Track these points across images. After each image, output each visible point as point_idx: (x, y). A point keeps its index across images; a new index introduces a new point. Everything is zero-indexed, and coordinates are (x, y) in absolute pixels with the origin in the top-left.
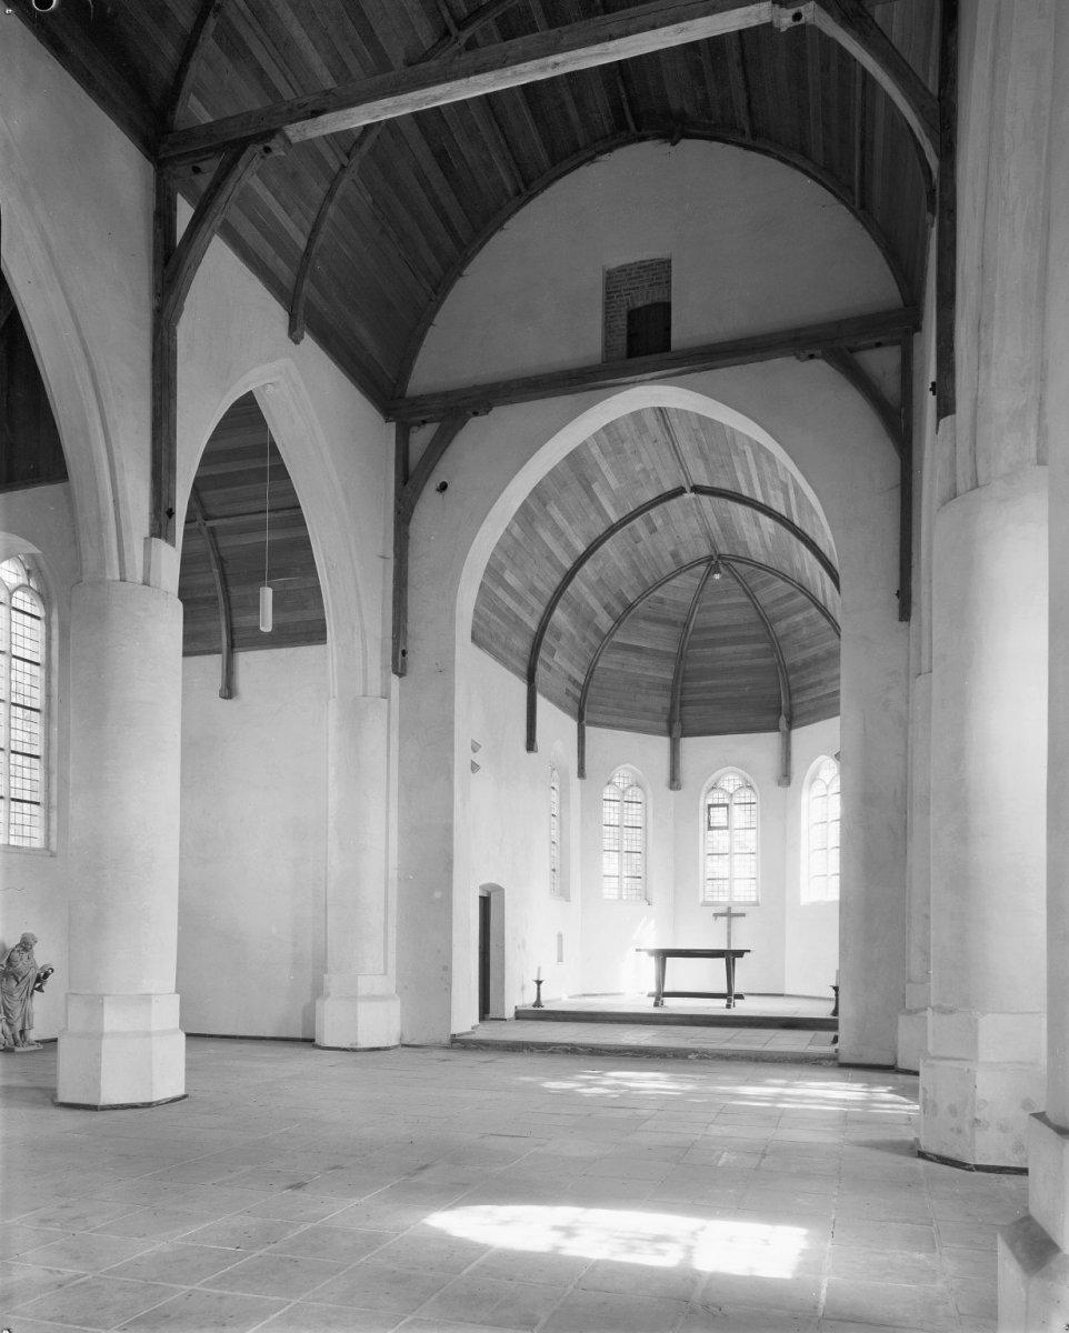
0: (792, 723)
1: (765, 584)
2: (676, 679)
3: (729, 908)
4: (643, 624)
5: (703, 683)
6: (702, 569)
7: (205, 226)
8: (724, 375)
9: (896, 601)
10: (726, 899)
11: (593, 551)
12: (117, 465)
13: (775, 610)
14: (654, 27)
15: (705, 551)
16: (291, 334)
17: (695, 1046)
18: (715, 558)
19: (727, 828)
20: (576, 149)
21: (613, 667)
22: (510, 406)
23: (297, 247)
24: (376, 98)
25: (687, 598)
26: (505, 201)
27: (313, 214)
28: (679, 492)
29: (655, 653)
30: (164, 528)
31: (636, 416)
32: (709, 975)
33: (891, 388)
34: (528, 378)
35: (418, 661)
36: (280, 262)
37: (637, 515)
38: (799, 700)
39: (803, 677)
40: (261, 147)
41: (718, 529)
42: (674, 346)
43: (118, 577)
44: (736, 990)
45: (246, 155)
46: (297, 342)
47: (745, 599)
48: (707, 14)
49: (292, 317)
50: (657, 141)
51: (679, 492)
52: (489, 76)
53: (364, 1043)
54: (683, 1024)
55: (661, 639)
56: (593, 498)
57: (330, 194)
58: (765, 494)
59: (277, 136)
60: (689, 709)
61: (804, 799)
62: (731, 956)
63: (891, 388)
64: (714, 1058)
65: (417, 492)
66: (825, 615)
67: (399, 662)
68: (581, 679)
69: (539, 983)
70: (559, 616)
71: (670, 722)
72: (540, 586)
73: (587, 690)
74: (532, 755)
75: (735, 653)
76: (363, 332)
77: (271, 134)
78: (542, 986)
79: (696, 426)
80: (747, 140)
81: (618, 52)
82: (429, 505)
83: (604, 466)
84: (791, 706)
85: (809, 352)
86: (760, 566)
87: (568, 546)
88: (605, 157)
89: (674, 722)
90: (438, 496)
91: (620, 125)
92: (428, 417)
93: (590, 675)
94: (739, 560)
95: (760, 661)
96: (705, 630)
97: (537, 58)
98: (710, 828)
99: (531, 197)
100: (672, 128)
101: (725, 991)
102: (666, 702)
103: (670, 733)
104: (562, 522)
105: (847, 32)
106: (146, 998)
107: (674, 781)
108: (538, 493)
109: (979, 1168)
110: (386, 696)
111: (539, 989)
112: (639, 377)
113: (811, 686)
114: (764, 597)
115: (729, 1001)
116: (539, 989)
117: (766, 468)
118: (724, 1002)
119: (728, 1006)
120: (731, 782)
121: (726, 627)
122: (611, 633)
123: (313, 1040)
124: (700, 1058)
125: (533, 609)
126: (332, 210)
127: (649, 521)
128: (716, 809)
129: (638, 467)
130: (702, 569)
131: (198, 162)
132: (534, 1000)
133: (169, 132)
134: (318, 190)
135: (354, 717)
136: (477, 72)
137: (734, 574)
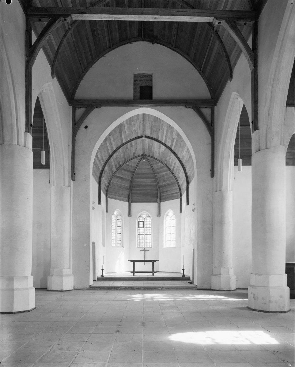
1: (156, 164)
2: (130, 187)
3: (144, 249)
4: (123, 171)
5: (137, 188)
6: (139, 158)
7: (44, 38)
8: (167, 108)
9: (210, 172)
10: (143, 246)
11: (117, 150)
13: (158, 171)
14: (184, 15)
15: (142, 153)
16: (52, 75)
17: (160, 286)
18: (144, 155)
19: (143, 227)
24: (102, 13)
25: (134, 165)
26: (106, 48)
27: (60, 40)
28: (142, 137)
31: (138, 116)
32: (148, 267)
33: (209, 119)
34: (113, 100)
35: (78, 177)
38: (163, 195)
39: (164, 189)
40: (63, 19)
41: (147, 148)
42: (154, 96)
43: (17, 144)
44: (155, 271)
45: (59, 20)
46: (53, 78)
47: (150, 167)
49: (52, 70)
50: (149, 42)
51: (142, 137)
52: (137, 16)
53: (65, 289)
54: (145, 280)
55: (127, 175)
57: (65, 36)
58: (166, 140)
59: (70, 16)
61: (164, 221)
62: (153, 261)
63: (209, 119)
64: (165, 289)
65: (79, 127)
66: (172, 173)
67: (73, 177)
69: (103, 270)
70: (106, 167)
71: (129, 198)
72: (104, 158)
73: (108, 188)
78: (103, 271)
79: (152, 120)
80: (173, 48)
82: (82, 131)
83: (126, 127)
86: (156, 159)
87: (112, 148)
88: (134, 43)
89: (130, 198)
90: (85, 130)
91: (140, 35)
92: (82, 106)
94: (150, 156)
95: (152, 184)
97: (152, 15)
98: (139, 227)
100: (153, 40)
101: (152, 271)
102: (128, 193)
103: (128, 201)
104: (112, 141)
105: (232, 30)
106: (26, 277)
107: (130, 214)
109: (271, 312)
110: (69, 186)
111: (102, 271)
113: (167, 191)
114: (155, 167)
115: (153, 274)
116: (102, 271)
117: (169, 134)
118: (152, 274)
119: (153, 275)
120: (144, 215)
121: (144, 174)
123: (47, 289)
124: (162, 289)
125: (101, 165)
126: (65, 41)
127: (132, 144)
128: (140, 222)
129: (133, 129)
130: (139, 158)
131: (41, 18)
132: (101, 274)
133: (31, 6)
135: (60, 193)
136: (134, 14)
137: (148, 160)
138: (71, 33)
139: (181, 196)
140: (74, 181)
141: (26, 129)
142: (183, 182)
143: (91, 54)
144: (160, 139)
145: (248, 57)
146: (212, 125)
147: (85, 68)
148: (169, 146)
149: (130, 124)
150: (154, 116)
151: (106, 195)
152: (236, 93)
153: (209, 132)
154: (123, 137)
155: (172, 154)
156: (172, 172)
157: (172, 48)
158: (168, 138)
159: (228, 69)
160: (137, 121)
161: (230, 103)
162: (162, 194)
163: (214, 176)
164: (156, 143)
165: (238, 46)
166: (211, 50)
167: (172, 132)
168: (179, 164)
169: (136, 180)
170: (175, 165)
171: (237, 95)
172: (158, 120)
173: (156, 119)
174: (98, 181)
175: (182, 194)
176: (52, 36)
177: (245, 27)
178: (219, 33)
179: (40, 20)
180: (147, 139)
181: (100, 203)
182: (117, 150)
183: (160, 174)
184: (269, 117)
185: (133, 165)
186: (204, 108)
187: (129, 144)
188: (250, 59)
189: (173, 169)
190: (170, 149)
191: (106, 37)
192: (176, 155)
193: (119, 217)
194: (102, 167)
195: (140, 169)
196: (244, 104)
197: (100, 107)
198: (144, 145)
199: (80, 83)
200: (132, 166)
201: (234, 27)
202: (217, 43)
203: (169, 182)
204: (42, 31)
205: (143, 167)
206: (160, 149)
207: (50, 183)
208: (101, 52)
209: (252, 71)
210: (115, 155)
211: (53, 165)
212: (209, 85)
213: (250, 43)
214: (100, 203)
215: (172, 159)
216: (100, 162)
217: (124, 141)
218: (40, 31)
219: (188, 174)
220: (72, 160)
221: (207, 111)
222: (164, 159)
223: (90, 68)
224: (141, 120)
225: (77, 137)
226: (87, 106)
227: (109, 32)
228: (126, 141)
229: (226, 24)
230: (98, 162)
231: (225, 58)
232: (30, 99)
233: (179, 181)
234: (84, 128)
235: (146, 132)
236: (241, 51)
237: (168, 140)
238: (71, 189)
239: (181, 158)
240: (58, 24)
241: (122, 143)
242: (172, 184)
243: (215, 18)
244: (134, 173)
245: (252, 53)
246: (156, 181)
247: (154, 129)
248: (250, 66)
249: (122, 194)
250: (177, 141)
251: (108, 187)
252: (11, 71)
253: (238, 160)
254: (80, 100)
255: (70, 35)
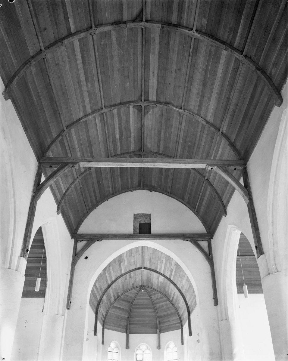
0: (161, 331)
1: (155, 294)
2: (128, 317)
4: (121, 302)
6: (138, 288)
7: (52, 179)
9: (213, 300)
12: (16, 234)
14: (180, 163)
15: (140, 284)
18: (143, 286)
20: (128, 188)
21: (112, 312)
22: (108, 240)
23: (63, 192)
27: (68, 186)
28: (141, 268)
29: (123, 310)
30: (25, 254)
31: (137, 248)
36: (58, 194)
37: (128, 273)
38: (163, 325)
42: (152, 232)
43: (8, 267)
45: (68, 166)
46: (58, 214)
47: (148, 298)
48: (192, 163)
49: (58, 207)
50: (147, 191)
51: (141, 268)
52: (138, 164)
56: (120, 266)
57: (73, 183)
58: (164, 271)
59: (77, 164)
60: (132, 326)
63: (207, 250)
65: (79, 258)
68: (104, 315)
70: (105, 297)
72: (102, 288)
74: (95, 336)
75: (145, 311)
76: (71, 216)
77: (76, 163)
79: (151, 252)
80: (169, 194)
81: (170, 166)
82: (81, 261)
83: (125, 259)
84: (160, 327)
85: (187, 239)
86: (154, 289)
87: (111, 278)
88: (135, 191)
92: (84, 239)
93: (107, 314)
94: (148, 287)
96: (137, 305)
99: (116, 195)
103: (126, 332)
104: (112, 272)
107: (127, 347)
108: (109, 265)
110: (63, 315)
112: (144, 238)
113: (166, 322)
114: (154, 297)
121: (143, 304)
122: (113, 303)
126: (73, 186)
127: (130, 275)
129: (133, 260)
133: (44, 157)
134: (71, 181)
137: (146, 290)
138: (79, 181)
139: (182, 326)
140: (69, 310)
141: (21, 253)
142: (184, 311)
143: (96, 199)
144: (158, 270)
145: (242, 192)
146: (210, 255)
147: (89, 210)
148: (168, 276)
149: (130, 256)
150: (153, 249)
151: (103, 326)
152: (232, 226)
153: (208, 262)
154: (123, 268)
155: (171, 284)
156: (171, 302)
157: (168, 194)
158: (166, 269)
159: (222, 207)
160: (136, 253)
161: (227, 234)
162: (161, 324)
163: (218, 304)
164: (155, 273)
165: (231, 185)
166: (204, 194)
167: (170, 263)
168: (179, 293)
169: (135, 310)
170: (174, 295)
171: (233, 227)
172: (157, 253)
173: (155, 251)
174: (95, 311)
175: (183, 325)
176: (60, 179)
177: (235, 171)
178: (210, 181)
179: (51, 166)
180: (146, 270)
181: (95, 334)
182: (116, 281)
183: (159, 305)
184: (274, 242)
185: (131, 295)
186: (200, 241)
187: (128, 275)
188: (244, 195)
189: (173, 299)
190: (169, 279)
191: (110, 186)
192: (175, 285)
193: (116, 350)
194: (100, 297)
195: (138, 299)
196: (242, 234)
197: (102, 240)
198: (143, 276)
199: (83, 220)
200: (130, 297)
201: (226, 171)
202: (209, 188)
203: (169, 312)
204: (51, 174)
205: (142, 298)
206: (159, 279)
207: (43, 312)
208: (104, 197)
209: (248, 204)
210: (113, 285)
211: (49, 293)
212: (204, 222)
213: (242, 181)
214: (95, 334)
215: (171, 290)
216: (98, 291)
217: (123, 273)
218: (49, 173)
219: (189, 304)
220: (69, 289)
221: (204, 244)
222: (162, 290)
223: (94, 209)
224: (140, 252)
225: (77, 267)
226: (88, 239)
227: (113, 182)
228: (125, 272)
229: (219, 169)
230: (96, 291)
231: (217, 199)
232: (30, 227)
233: (179, 311)
234: (85, 258)
235: (145, 264)
236: (234, 189)
237: (167, 271)
238: (64, 319)
239: (180, 288)
240: (66, 170)
241: (121, 274)
242: (172, 314)
243: (207, 164)
244: (133, 303)
245: (245, 189)
246: (155, 312)
247: (153, 260)
248: (245, 200)
249: (120, 325)
250: (176, 271)
251: (105, 318)
252: (15, 202)
253: (243, 286)
254: (82, 234)
255: (78, 183)
